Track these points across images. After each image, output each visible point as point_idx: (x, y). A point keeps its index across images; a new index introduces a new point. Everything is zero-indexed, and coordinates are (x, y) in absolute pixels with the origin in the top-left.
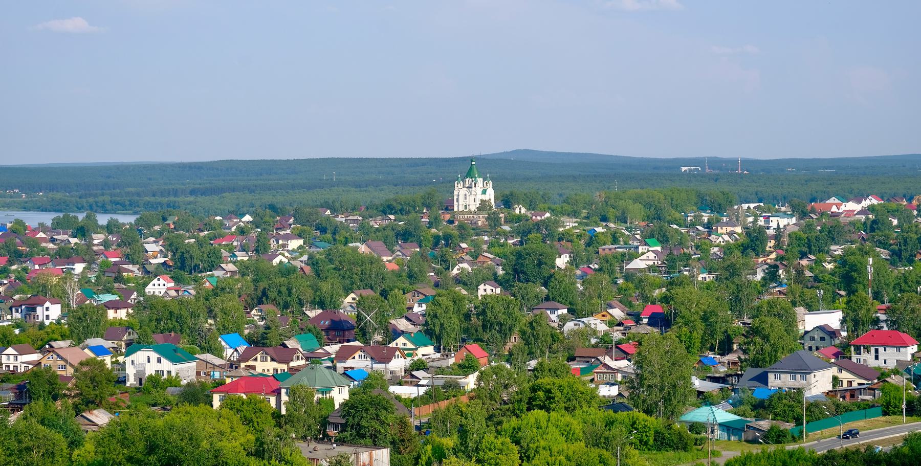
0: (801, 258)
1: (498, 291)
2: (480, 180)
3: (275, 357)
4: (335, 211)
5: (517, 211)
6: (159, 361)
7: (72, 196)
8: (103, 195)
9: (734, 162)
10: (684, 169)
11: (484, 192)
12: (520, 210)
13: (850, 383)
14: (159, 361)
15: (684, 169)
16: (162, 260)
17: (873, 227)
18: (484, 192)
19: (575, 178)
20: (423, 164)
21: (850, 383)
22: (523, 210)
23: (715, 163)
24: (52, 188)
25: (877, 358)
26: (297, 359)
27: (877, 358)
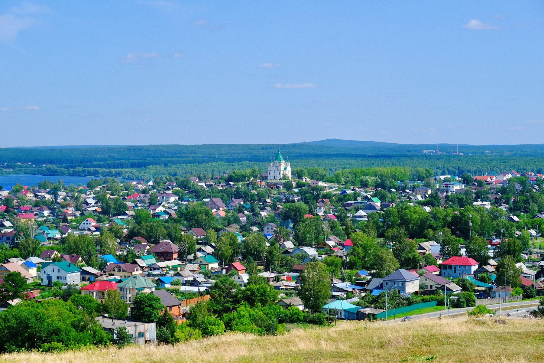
0: (99, 292)
1: (463, 187)
2: (283, 162)
3: (125, 269)
4: (200, 180)
5: (304, 180)
6: (59, 271)
7: (61, 167)
8: (79, 166)
9: (454, 147)
10: (425, 151)
11: (285, 169)
12: (306, 180)
13: (431, 287)
14: (59, 271)
15: (425, 151)
16: (94, 209)
17: (503, 191)
18: (285, 169)
19: (364, 156)
20: (271, 148)
21: (431, 287)
22: (308, 179)
23: (443, 147)
24: (52, 162)
25: (455, 272)
26: (137, 270)
27: (455, 272)
